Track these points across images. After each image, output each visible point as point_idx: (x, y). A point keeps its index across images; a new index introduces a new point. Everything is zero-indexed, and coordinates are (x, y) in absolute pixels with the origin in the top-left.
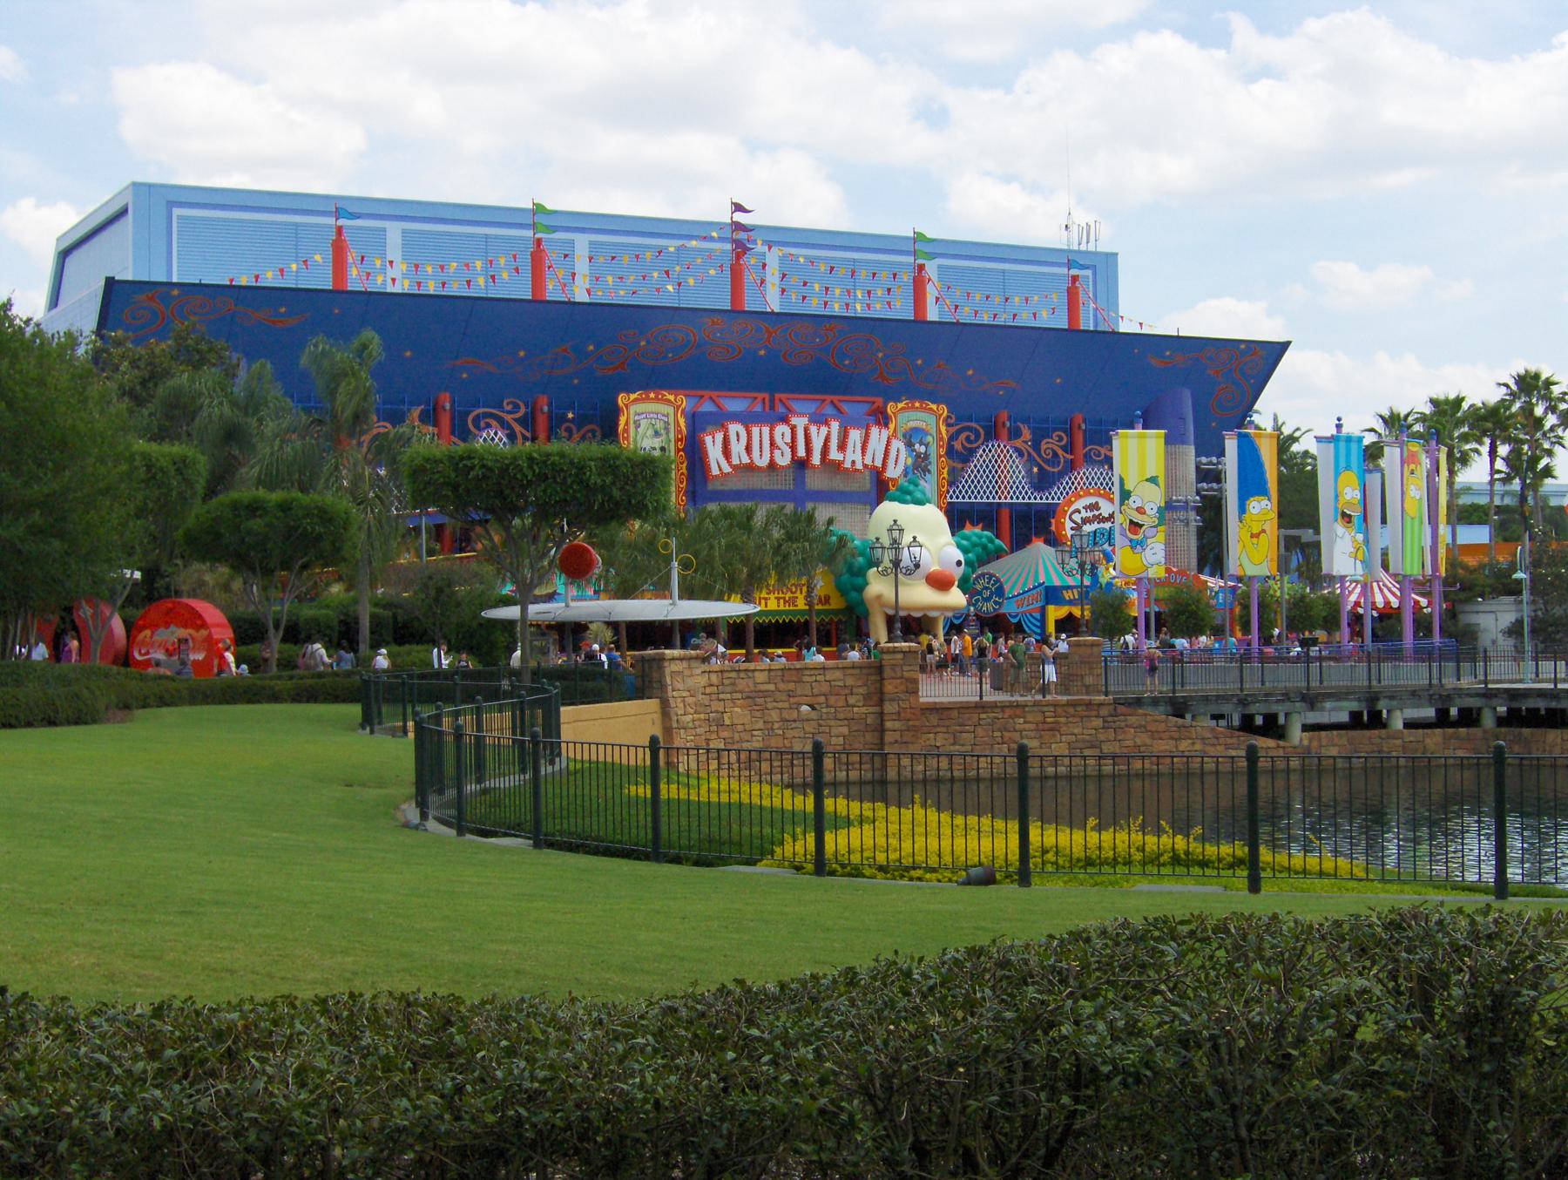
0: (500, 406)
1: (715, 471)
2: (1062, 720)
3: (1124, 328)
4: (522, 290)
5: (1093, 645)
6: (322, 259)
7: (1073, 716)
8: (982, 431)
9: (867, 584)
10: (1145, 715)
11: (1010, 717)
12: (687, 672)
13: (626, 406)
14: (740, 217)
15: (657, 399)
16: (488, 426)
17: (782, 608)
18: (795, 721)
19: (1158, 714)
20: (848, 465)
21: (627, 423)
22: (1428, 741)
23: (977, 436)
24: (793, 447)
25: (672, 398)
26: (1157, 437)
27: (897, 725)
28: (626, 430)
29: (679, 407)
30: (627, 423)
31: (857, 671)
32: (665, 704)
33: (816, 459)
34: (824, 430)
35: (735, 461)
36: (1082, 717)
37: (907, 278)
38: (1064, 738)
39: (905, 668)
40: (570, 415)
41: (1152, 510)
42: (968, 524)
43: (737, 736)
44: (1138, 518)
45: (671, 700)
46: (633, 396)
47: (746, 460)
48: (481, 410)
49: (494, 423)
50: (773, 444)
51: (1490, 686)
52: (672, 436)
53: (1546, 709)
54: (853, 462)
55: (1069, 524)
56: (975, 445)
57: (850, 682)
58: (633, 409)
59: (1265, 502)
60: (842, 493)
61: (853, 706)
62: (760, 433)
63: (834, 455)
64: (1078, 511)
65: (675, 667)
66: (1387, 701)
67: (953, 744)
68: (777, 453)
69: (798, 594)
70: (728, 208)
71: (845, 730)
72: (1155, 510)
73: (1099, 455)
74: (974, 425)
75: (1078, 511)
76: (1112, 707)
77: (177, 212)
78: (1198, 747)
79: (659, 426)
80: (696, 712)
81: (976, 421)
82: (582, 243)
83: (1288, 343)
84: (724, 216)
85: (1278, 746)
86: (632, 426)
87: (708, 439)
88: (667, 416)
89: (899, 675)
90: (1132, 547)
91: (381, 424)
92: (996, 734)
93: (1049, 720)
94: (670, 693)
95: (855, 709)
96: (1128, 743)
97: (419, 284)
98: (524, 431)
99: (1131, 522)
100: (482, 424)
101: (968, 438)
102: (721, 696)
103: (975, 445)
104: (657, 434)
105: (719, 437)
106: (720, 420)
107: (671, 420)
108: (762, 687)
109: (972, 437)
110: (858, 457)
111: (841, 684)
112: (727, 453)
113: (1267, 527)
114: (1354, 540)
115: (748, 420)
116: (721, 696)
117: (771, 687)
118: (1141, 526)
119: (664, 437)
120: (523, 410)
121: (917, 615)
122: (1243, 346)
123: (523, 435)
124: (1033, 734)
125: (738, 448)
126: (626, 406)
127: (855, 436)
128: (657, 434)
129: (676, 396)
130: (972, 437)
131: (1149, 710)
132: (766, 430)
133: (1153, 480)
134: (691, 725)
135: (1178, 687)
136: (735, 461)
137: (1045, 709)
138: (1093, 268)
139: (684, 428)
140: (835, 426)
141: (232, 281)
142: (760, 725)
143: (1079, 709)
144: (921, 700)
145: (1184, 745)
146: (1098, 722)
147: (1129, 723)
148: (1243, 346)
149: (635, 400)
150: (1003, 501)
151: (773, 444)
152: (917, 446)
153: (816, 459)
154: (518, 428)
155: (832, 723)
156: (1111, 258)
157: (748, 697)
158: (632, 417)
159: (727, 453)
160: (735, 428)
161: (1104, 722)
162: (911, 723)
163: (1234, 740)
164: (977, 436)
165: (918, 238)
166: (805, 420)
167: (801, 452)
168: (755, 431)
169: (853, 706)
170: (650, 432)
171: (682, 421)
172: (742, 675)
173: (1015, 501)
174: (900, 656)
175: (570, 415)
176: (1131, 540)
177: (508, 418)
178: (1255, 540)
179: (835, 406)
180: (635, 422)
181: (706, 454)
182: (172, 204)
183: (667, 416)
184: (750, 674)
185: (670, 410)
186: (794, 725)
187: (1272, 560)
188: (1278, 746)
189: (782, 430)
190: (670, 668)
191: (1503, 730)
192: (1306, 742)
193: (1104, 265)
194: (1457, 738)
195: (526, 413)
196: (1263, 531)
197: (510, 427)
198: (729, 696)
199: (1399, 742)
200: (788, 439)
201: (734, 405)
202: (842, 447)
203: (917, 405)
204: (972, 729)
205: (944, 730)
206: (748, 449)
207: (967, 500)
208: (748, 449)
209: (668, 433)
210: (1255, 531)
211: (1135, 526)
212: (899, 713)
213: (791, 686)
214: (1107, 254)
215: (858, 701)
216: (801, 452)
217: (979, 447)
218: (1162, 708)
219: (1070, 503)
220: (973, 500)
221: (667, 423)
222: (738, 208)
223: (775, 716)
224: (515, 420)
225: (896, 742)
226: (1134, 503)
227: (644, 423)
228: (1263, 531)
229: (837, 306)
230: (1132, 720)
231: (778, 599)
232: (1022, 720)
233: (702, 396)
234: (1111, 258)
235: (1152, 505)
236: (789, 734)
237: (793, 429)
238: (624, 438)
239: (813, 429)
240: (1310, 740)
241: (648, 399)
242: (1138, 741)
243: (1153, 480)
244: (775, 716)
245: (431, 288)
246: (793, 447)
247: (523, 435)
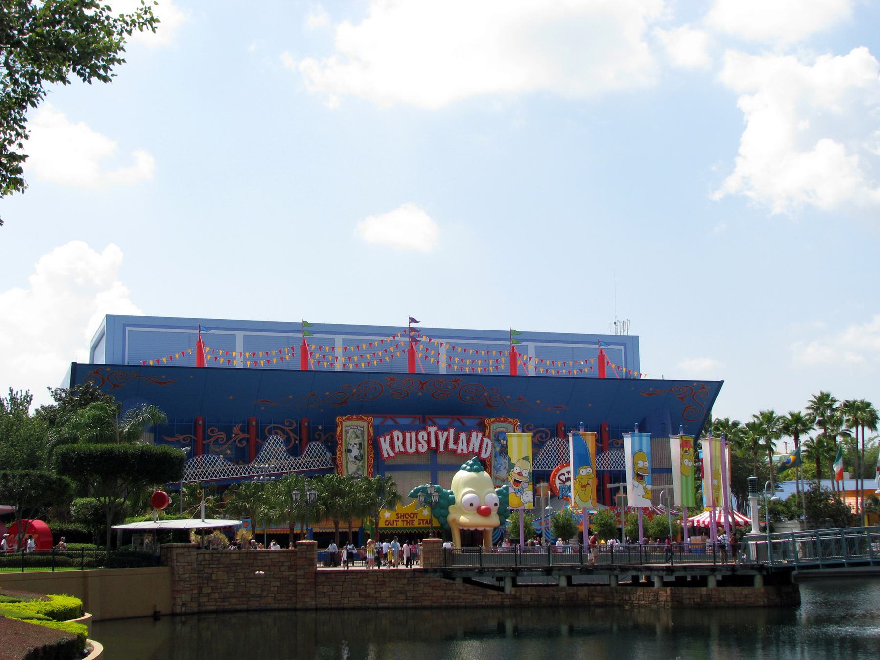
0: (283, 424)
1: (386, 455)
2: (388, 580)
3: (643, 378)
4: (297, 365)
5: (434, 542)
6: (192, 352)
7: (392, 578)
8: (549, 432)
9: (448, 513)
10: (429, 578)
11: (360, 578)
12: (186, 554)
13: (341, 422)
14: (413, 325)
15: (357, 419)
16: (276, 433)
17: (405, 525)
18: (252, 579)
19: (436, 577)
20: (459, 451)
21: (341, 431)
22: (579, 593)
23: (547, 435)
24: (429, 442)
25: (365, 418)
26: (528, 436)
27: (303, 581)
28: (341, 435)
29: (369, 423)
30: (341, 431)
31: (286, 554)
32: (172, 568)
33: (441, 449)
34: (446, 434)
35: (397, 450)
36: (397, 578)
37: (507, 353)
38: (387, 589)
39: (308, 553)
40: (320, 428)
41: (526, 473)
42: (541, 481)
43: (219, 586)
44: (518, 478)
45: (176, 567)
46: (344, 418)
47: (402, 449)
48: (273, 425)
49: (280, 432)
50: (417, 441)
51: (716, 564)
52: (366, 437)
53: (700, 577)
54: (462, 450)
55: (558, 481)
56: (545, 440)
57: (282, 559)
58: (344, 424)
59: (589, 470)
60: (401, 466)
61: (283, 572)
62: (411, 436)
63: (452, 446)
64: (564, 474)
65: (179, 551)
66: (557, 571)
67: (332, 591)
68: (420, 446)
69: (415, 518)
70: (408, 320)
71: (278, 584)
72: (528, 474)
73: (618, 444)
74: (544, 429)
75: (564, 474)
76: (412, 573)
77: (128, 329)
78: (456, 594)
79: (358, 432)
80: (191, 573)
81: (545, 427)
82: (339, 340)
83: (722, 382)
84: (405, 324)
85: (499, 594)
86: (344, 433)
87: (382, 439)
88: (363, 427)
89: (304, 556)
90: (515, 493)
91: (220, 433)
92: (353, 586)
93: (380, 580)
94: (175, 564)
95: (284, 573)
96: (420, 592)
97: (255, 363)
98: (296, 436)
99: (515, 480)
100: (273, 432)
101: (541, 436)
102: (211, 566)
103: (545, 440)
104: (357, 437)
105: (388, 438)
106: (389, 430)
107: (365, 429)
108: (235, 562)
109: (544, 436)
110: (465, 447)
111: (277, 560)
112: (392, 445)
113: (590, 482)
114: (645, 488)
115: (404, 430)
116: (211, 566)
117: (240, 562)
118: (520, 482)
119: (361, 438)
120: (295, 425)
121: (472, 529)
122: (695, 384)
123: (295, 438)
124: (372, 587)
125: (398, 445)
126: (341, 422)
127: (463, 436)
128: (357, 437)
129: (368, 417)
130: (544, 436)
131: (432, 575)
132: (413, 434)
133: (526, 458)
134: (188, 579)
135: (518, 564)
136: (397, 450)
137: (379, 574)
138: (624, 344)
139: (372, 433)
140: (452, 431)
141: (144, 363)
142: (233, 580)
143: (395, 574)
144: (318, 569)
145: (449, 593)
146: (405, 581)
147: (421, 581)
148: (695, 384)
149: (346, 420)
150: (606, 469)
151: (417, 441)
152: (502, 441)
153: (441, 449)
154: (292, 435)
155: (272, 580)
156: (635, 339)
157: (227, 567)
158: (344, 428)
159: (392, 445)
160: (396, 433)
161: (408, 581)
162: (310, 580)
163: (476, 591)
164: (547, 435)
165: (512, 332)
166: (435, 429)
167: (433, 445)
168: (408, 434)
169: (283, 572)
170: (354, 436)
171: (371, 430)
172: (224, 555)
173: (612, 469)
174: (305, 547)
175: (320, 428)
176: (515, 490)
177: (287, 429)
178: (584, 489)
179: (459, 421)
180: (345, 431)
181: (381, 448)
182: (125, 326)
183: (363, 427)
184: (229, 555)
185: (365, 424)
186: (251, 581)
187: (593, 499)
188: (499, 594)
189: (423, 434)
190: (175, 552)
191: (720, 588)
192: (513, 593)
193: (630, 344)
194: (596, 591)
195: (296, 427)
196: (588, 484)
197: (287, 434)
198: (215, 566)
199: (563, 593)
200: (426, 438)
201: (404, 421)
202: (456, 442)
203: (502, 419)
204: (341, 583)
205: (327, 584)
206: (404, 444)
207: (540, 469)
208: (404, 444)
209: (363, 437)
210: (583, 484)
211: (517, 482)
212: (304, 575)
213: (251, 561)
214: (633, 337)
215: (285, 569)
216: (433, 445)
217: (547, 441)
218: (438, 574)
219: (558, 470)
220: (543, 469)
221: (363, 431)
222: (412, 320)
223: (241, 576)
224: (291, 430)
225: (303, 589)
226: (516, 470)
227: (350, 431)
228: (588, 484)
229: (467, 369)
230: (422, 580)
231: (403, 521)
232: (366, 580)
233: (386, 417)
234: (635, 339)
235: (526, 471)
236: (248, 585)
237: (429, 434)
238: (339, 439)
239: (440, 433)
240: (516, 592)
241: (352, 419)
242: (426, 591)
243: (526, 458)
244: (241, 576)
245: (262, 364)
246: (429, 442)
247: (295, 438)
